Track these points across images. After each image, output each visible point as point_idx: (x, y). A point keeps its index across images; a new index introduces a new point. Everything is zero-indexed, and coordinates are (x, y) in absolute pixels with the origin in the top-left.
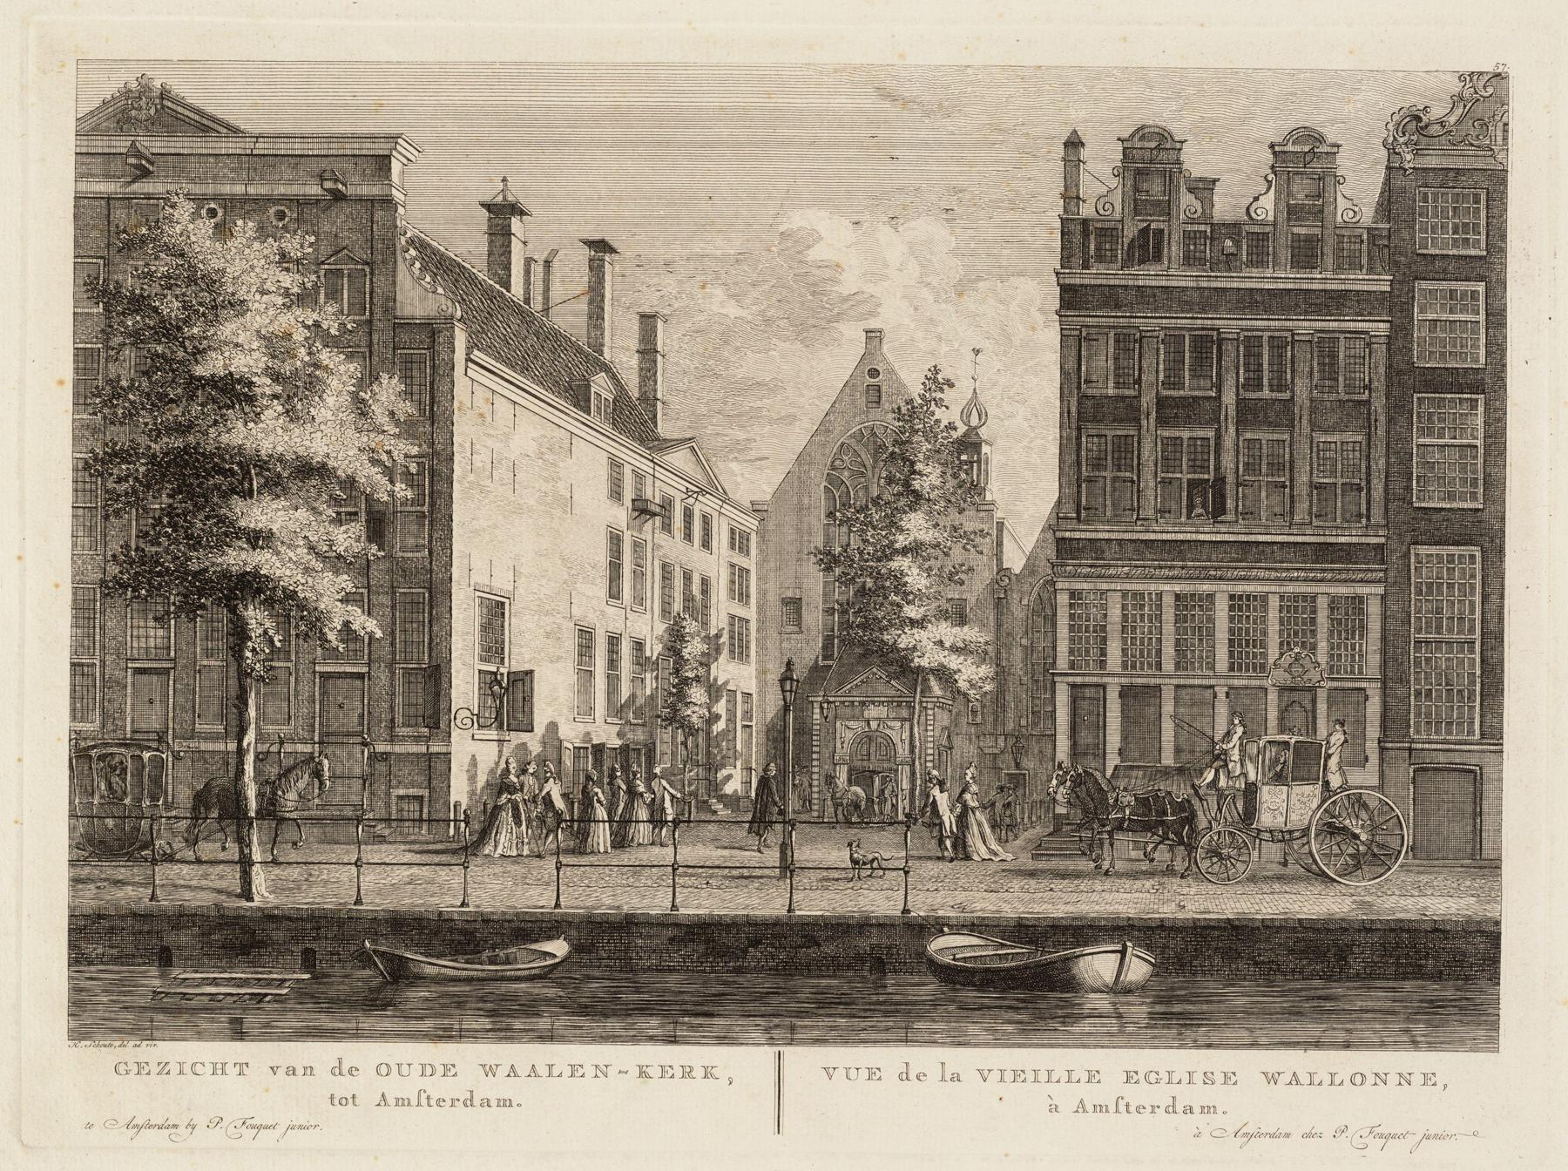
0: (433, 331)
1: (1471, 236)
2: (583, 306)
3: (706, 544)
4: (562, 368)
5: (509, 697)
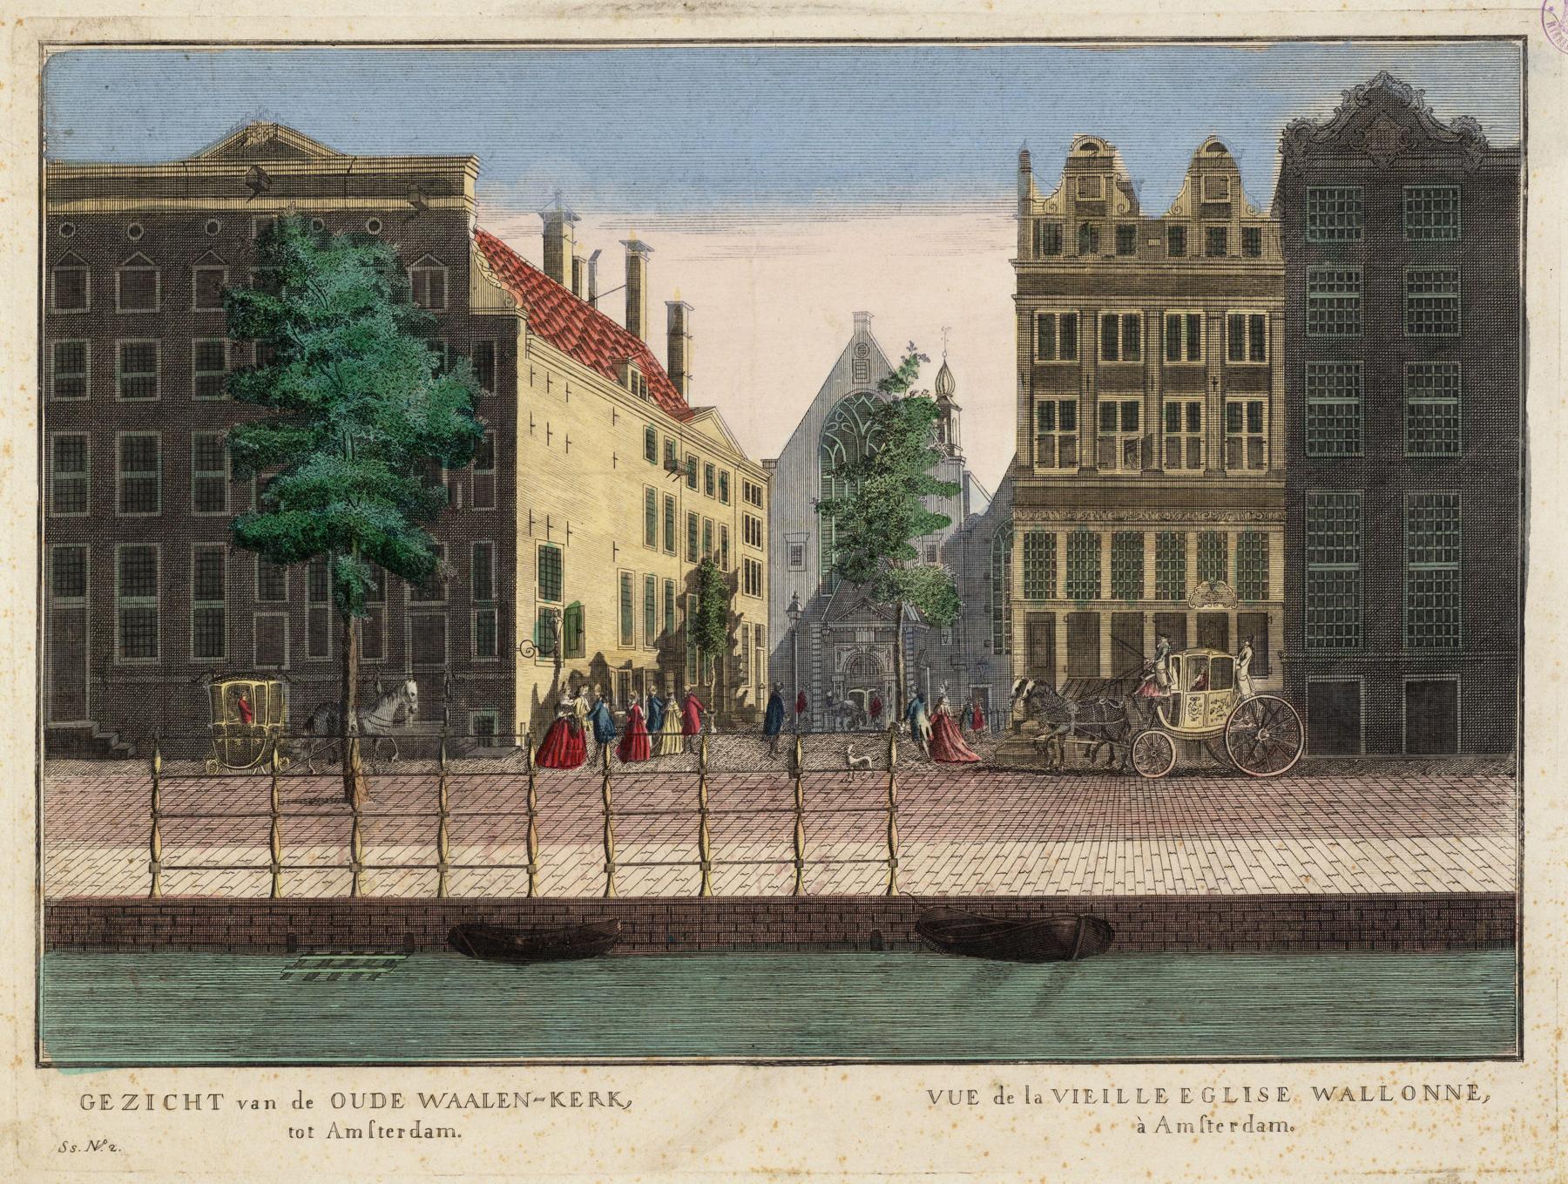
0: (505, 326)
1: (1414, 198)
2: (622, 296)
3: (725, 497)
4: (606, 347)
5: (559, 634)
